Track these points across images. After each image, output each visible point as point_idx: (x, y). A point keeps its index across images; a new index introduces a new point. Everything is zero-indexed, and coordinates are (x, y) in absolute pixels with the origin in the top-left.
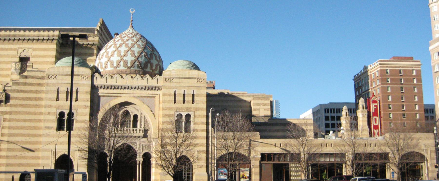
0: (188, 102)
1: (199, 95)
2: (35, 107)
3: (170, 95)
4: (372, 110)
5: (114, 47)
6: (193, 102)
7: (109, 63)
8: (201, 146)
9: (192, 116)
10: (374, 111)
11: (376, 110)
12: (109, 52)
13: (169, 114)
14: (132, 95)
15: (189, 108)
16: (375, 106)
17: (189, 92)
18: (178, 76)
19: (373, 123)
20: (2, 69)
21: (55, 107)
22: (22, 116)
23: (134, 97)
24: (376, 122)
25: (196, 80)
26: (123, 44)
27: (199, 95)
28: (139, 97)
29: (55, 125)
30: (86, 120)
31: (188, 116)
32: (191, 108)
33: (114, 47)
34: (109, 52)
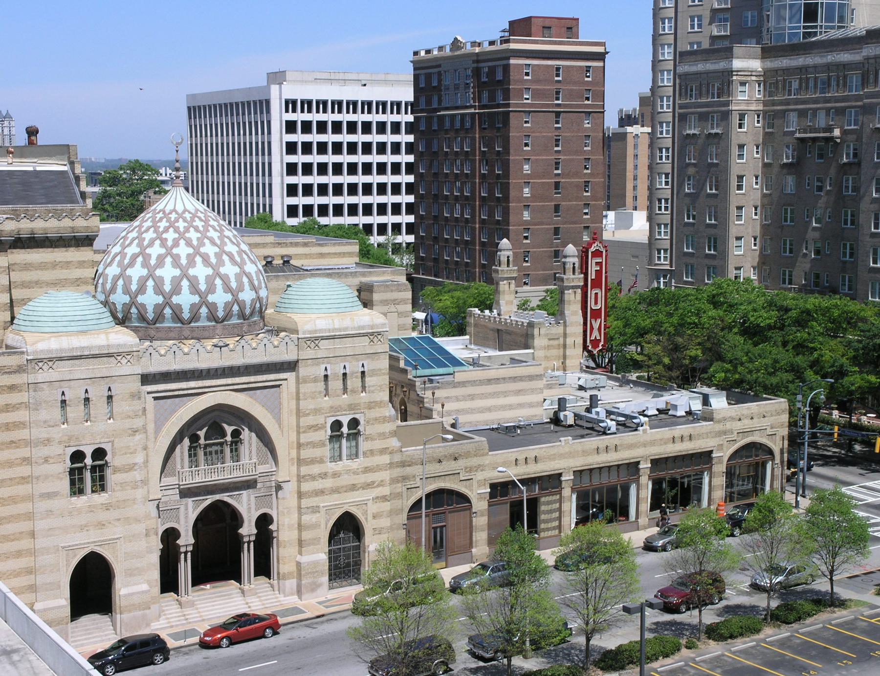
0: (354, 391)
1: (374, 372)
2: (8, 448)
3: (315, 380)
4: (592, 275)
6: (364, 388)
7: (150, 283)
8: (378, 486)
9: (362, 422)
10: (593, 277)
11: (599, 273)
12: (150, 255)
13: (315, 423)
16: (597, 263)
17: (353, 367)
19: (591, 304)
20: (6, 538)
21: (60, 443)
24: (596, 303)
27: (374, 372)
29: (65, 484)
31: (354, 423)
32: (359, 404)
34: (150, 255)
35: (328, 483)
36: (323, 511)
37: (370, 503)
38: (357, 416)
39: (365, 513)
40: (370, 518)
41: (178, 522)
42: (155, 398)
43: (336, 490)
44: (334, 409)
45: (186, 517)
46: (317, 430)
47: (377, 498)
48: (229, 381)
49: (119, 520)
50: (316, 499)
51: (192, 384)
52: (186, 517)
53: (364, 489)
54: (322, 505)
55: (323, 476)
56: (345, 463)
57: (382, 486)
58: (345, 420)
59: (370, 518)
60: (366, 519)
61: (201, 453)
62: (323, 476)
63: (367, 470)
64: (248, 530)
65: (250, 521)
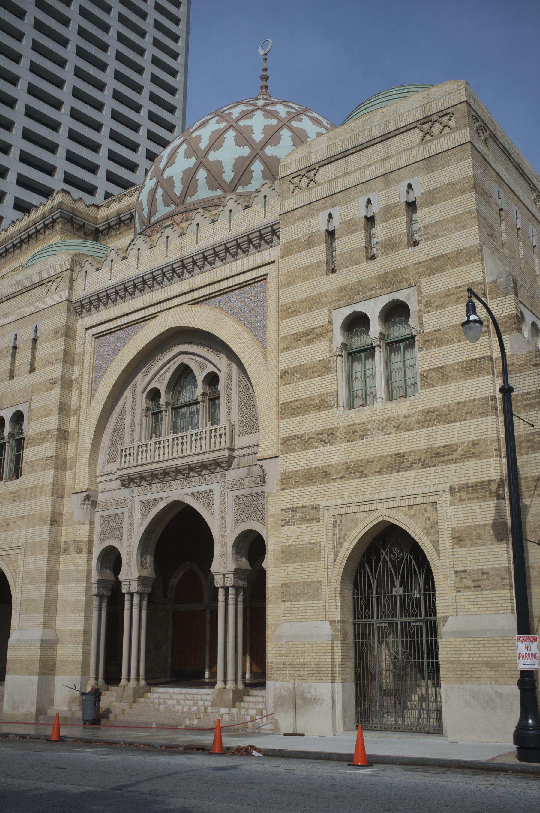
5: (187, 156)
8: (467, 456)
9: (413, 307)
13: (309, 327)
14: (189, 297)
15: (395, 273)
18: (339, 150)
22: (337, 719)
23: (195, 302)
25: (416, 135)
26: (226, 130)
28: (210, 297)
30: (48, 432)
31: (396, 312)
32: (404, 269)
33: (187, 156)
35: (337, 454)
36: (326, 517)
37: (444, 502)
38: (400, 296)
39: (432, 528)
40: (446, 541)
41: (120, 539)
42: (98, 336)
43: (356, 470)
44: (357, 292)
45: (130, 531)
46: (312, 341)
47: (465, 487)
48: (186, 284)
49: (23, 517)
50: (312, 489)
51: (139, 301)
52: (130, 531)
53: (425, 465)
54: (323, 504)
55: (328, 437)
56: (380, 408)
57: (477, 455)
58: (373, 309)
59: (446, 541)
60: (436, 544)
61: (166, 419)
62: (328, 437)
63: (432, 418)
64: (224, 564)
65: (223, 544)
